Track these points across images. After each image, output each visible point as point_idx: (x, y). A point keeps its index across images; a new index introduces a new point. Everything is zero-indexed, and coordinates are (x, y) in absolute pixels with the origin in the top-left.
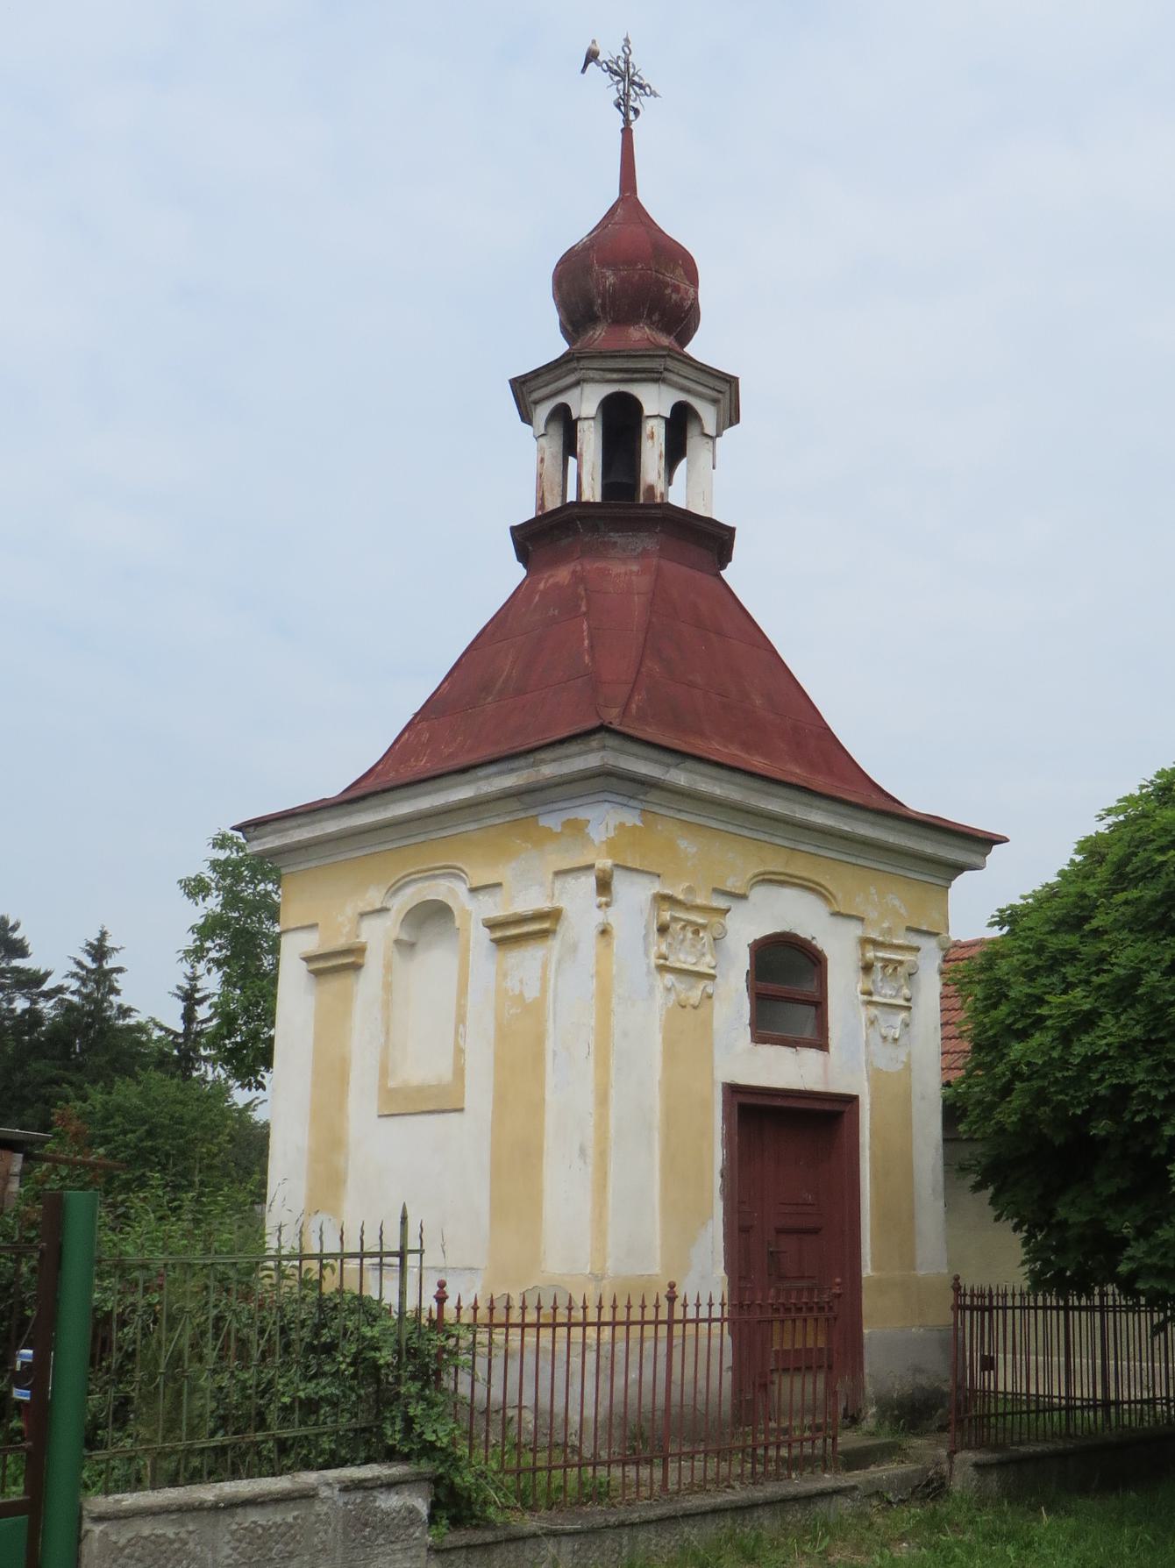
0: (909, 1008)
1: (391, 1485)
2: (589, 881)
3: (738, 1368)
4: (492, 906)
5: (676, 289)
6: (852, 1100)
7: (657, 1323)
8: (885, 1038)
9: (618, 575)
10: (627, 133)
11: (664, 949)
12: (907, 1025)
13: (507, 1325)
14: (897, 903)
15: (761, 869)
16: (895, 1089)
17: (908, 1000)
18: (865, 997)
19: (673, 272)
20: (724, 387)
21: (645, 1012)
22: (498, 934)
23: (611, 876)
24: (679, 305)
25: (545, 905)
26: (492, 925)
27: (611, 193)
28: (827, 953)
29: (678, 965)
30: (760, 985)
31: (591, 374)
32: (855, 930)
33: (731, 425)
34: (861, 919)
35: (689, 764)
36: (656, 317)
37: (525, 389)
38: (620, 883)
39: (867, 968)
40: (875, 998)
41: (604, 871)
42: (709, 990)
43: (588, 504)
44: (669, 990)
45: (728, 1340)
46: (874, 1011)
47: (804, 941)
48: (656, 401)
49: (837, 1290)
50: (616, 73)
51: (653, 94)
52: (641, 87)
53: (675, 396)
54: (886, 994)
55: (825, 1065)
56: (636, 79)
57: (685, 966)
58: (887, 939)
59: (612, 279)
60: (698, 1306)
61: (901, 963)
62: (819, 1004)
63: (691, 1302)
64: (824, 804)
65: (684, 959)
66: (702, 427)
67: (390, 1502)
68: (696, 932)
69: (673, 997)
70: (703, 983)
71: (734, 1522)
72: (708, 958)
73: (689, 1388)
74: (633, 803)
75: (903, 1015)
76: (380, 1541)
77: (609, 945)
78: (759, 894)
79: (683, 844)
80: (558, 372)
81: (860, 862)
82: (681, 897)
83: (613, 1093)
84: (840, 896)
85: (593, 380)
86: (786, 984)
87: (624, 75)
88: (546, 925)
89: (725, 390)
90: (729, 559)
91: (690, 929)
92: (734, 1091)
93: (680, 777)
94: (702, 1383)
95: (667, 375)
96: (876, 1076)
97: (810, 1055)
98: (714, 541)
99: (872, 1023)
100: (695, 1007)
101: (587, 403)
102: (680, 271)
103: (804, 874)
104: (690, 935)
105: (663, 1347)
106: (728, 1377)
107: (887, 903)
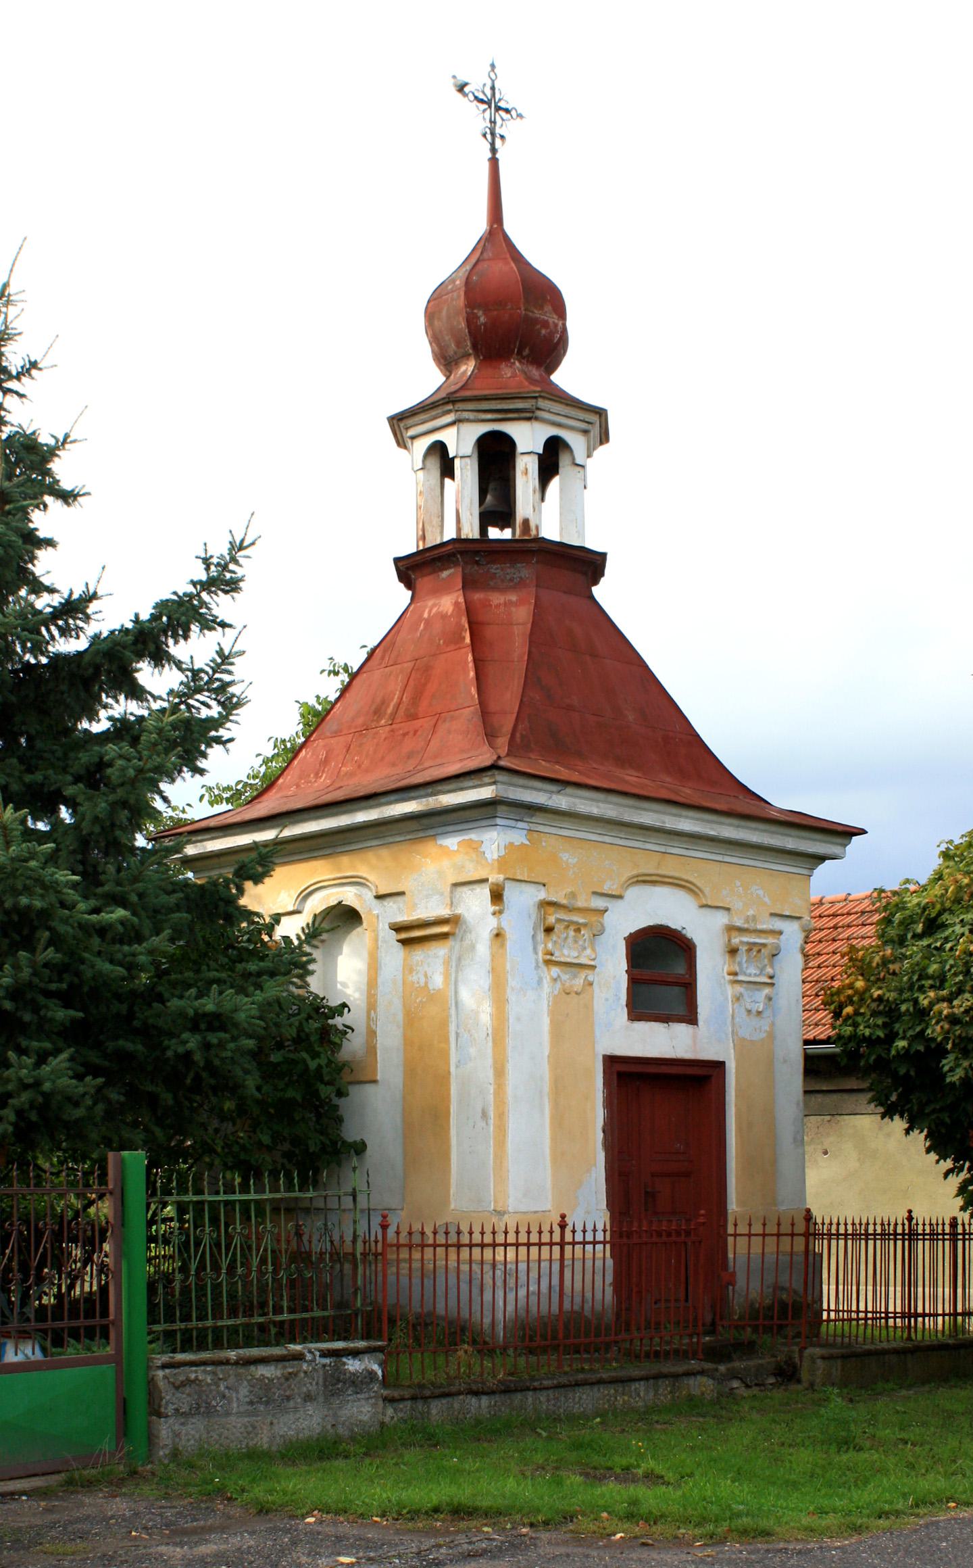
0: (773, 984)
1: (355, 1353)
2: (484, 892)
3: (617, 1285)
4: (399, 912)
5: (545, 324)
6: (720, 1066)
7: (551, 1244)
8: (749, 1012)
9: (498, 606)
10: (494, 163)
11: (550, 946)
12: (770, 999)
13: (435, 1246)
14: (761, 892)
15: (635, 872)
16: (759, 1054)
17: (771, 977)
18: (731, 977)
19: (541, 308)
20: (594, 418)
21: (533, 1004)
22: (404, 936)
23: (503, 889)
24: (548, 340)
25: (445, 912)
26: (398, 928)
27: (479, 225)
28: (696, 940)
29: (562, 959)
30: (635, 971)
31: (466, 415)
32: (721, 919)
33: (601, 443)
34: (728, 909)
35: (569, 790)
36: (526, 352)
37: (400, 423)
38: (512, 894)
39: (733, 952)
40: (740, 978)
41: (497, 885)
42: (590, 978)
43: (467, 541)
44: (555, 980)
45: (610, 1262)
46: (739, 989)
47: (675, 931)
48: (528, 439)
49: (701, 1220)
50: (482, 101)
51: (520, 116)
52: (507, 111)
53: (547, 432)
54: (751, 972)
55: (695, 1037)
56: (502, 104)
57: (569, 960)
58: (751, 926)
59: (482, 319)
60: (584, 1231)
61: (764, 945)
62: (689, 986)
63: (579, 1228)
64: (691, 813)
65: (568, 954)
66: (574, 459)
67: (353, 1365)
68: (578, 930)
69: (558, 985)
70: (583, 974)
71: (616, 1391)
72: (589, 951)
73: (578, 1299)
74: (520, 825)
75: (767, 991)
76: (349, 1392)
77: (503, 945)
78: (633, 893)
79: (565, 856)
80: (434, 413)
81: (727, 859)
82: (564, 902)
83: (510, 1067)
84: (707, 890)
85: (468, 420)
86: (661, 973)
87: (491, 103)
88: (445, 929)
89: (596, 423)
90: (602, 575)
91: (572, 928)
92: (611, 1061)
93: (561, 800)
94: (588, 1295)
95: (539, 413)
96: (742, 1046)
97: (681, 1029)
98: (590, 565)
99: (738, 999)
100: (577, 993)
101: (461, 440)
102: (548, 308)
103: (676, 874)
104: (572, 933)
105: (556, 1267)
106: (609, 1290)
107: (754, 892)
